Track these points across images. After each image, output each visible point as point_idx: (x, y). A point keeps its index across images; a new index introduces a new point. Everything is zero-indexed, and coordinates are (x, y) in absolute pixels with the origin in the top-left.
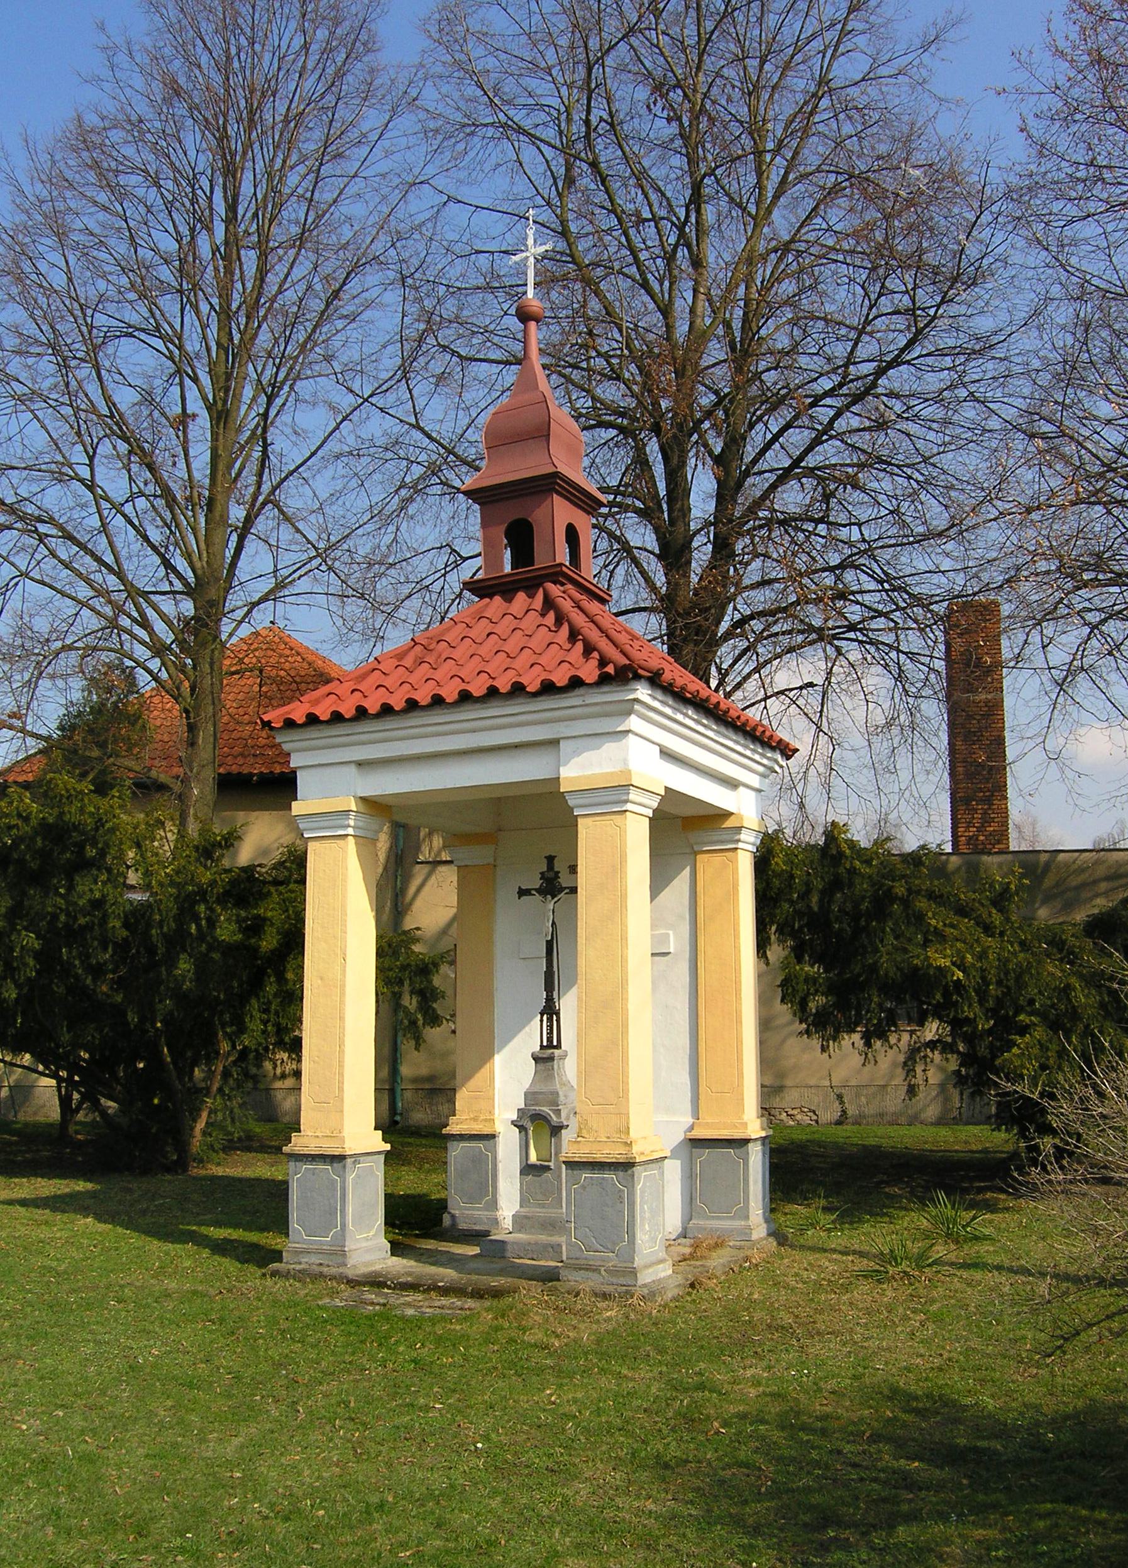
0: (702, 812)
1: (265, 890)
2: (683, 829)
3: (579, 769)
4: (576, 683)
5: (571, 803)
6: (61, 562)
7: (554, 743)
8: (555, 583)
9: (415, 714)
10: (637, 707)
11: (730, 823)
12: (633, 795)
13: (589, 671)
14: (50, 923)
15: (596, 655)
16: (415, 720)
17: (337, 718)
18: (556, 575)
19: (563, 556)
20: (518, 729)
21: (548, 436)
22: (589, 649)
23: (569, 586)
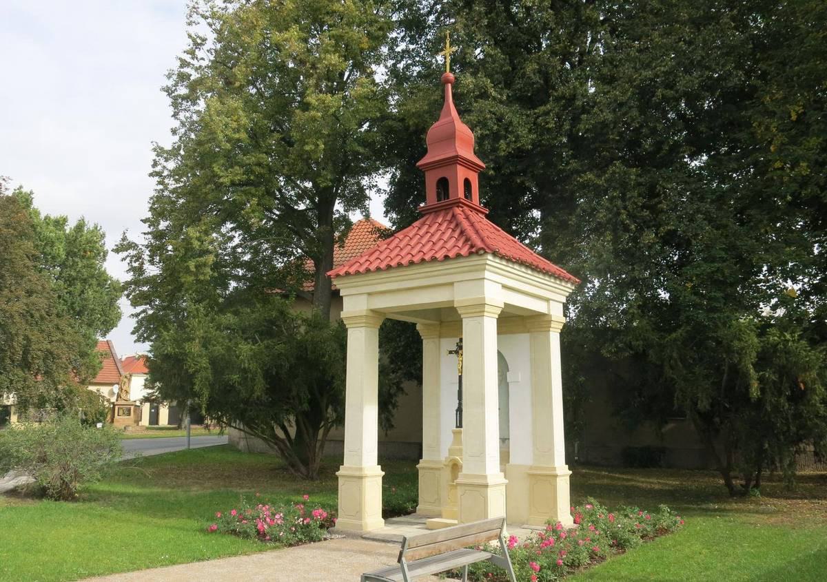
0: (531, 314)
1: (152, 228)
2: (514, 321)
3: (459, 296)
4: (458, 256)
5: (459, 312)
6: (403, 547)
7: (452, 284)
8: (458, 207)
9: (401, 270)
10: (487, 267)
11: (546, 319)
12: (487, 308)
13: (464, 251)
14: (490, 13)
15: (469, 243)
16: (371, 277)
17: (358, 273)
18: (458, 203)
19: (461, 194)
20: (493, 274)
21: (455, 138)
22: (467, 240)
23: (465, 208)
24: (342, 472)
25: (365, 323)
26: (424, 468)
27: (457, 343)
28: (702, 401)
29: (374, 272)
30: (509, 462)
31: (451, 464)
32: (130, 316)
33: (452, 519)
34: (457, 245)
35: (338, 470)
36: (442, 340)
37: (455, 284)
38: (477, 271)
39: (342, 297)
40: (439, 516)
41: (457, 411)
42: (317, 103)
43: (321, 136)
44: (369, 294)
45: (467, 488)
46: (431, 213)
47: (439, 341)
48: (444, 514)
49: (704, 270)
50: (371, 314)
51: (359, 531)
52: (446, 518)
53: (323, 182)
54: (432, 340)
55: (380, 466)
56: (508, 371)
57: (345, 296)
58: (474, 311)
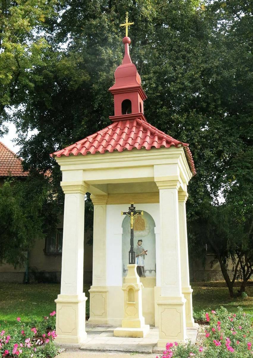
7: (152, 166)
24: (60, 299)
25: (80, 190)
26: (94, 292)
27: (130, 208)
28: (244, 245)
29: (111, 153)
30: (156, 286)
31: (128, 290)
32: (17, 145)
33: (128, 327)
34: (154, 140)
35: (56, 298)
36: (108, 206)
37: (154, 166)
38: (172, 158)
39: (61, 171)
40: (120, 326)
41: (129, 252)
42: (11, 48)
43: (10, 70)
44: (84, 170)
45: (166, 307)
46: (127, 120)
47: (106, 206)
48: (122, 326)
49: (241, 173)
50: (84, 184)
51: (76, 344)
52: (125, 327)
53: (4, 101)
54: (100, 206)
55: (84, 293)
56: (155, 226)
57: (64, 171)
58: (169, 184)
